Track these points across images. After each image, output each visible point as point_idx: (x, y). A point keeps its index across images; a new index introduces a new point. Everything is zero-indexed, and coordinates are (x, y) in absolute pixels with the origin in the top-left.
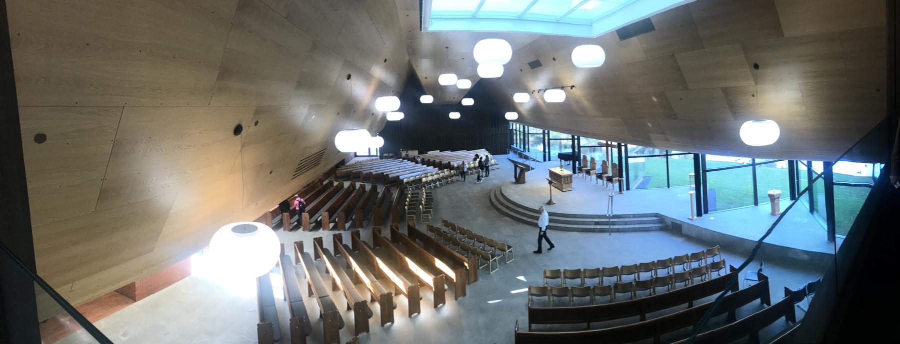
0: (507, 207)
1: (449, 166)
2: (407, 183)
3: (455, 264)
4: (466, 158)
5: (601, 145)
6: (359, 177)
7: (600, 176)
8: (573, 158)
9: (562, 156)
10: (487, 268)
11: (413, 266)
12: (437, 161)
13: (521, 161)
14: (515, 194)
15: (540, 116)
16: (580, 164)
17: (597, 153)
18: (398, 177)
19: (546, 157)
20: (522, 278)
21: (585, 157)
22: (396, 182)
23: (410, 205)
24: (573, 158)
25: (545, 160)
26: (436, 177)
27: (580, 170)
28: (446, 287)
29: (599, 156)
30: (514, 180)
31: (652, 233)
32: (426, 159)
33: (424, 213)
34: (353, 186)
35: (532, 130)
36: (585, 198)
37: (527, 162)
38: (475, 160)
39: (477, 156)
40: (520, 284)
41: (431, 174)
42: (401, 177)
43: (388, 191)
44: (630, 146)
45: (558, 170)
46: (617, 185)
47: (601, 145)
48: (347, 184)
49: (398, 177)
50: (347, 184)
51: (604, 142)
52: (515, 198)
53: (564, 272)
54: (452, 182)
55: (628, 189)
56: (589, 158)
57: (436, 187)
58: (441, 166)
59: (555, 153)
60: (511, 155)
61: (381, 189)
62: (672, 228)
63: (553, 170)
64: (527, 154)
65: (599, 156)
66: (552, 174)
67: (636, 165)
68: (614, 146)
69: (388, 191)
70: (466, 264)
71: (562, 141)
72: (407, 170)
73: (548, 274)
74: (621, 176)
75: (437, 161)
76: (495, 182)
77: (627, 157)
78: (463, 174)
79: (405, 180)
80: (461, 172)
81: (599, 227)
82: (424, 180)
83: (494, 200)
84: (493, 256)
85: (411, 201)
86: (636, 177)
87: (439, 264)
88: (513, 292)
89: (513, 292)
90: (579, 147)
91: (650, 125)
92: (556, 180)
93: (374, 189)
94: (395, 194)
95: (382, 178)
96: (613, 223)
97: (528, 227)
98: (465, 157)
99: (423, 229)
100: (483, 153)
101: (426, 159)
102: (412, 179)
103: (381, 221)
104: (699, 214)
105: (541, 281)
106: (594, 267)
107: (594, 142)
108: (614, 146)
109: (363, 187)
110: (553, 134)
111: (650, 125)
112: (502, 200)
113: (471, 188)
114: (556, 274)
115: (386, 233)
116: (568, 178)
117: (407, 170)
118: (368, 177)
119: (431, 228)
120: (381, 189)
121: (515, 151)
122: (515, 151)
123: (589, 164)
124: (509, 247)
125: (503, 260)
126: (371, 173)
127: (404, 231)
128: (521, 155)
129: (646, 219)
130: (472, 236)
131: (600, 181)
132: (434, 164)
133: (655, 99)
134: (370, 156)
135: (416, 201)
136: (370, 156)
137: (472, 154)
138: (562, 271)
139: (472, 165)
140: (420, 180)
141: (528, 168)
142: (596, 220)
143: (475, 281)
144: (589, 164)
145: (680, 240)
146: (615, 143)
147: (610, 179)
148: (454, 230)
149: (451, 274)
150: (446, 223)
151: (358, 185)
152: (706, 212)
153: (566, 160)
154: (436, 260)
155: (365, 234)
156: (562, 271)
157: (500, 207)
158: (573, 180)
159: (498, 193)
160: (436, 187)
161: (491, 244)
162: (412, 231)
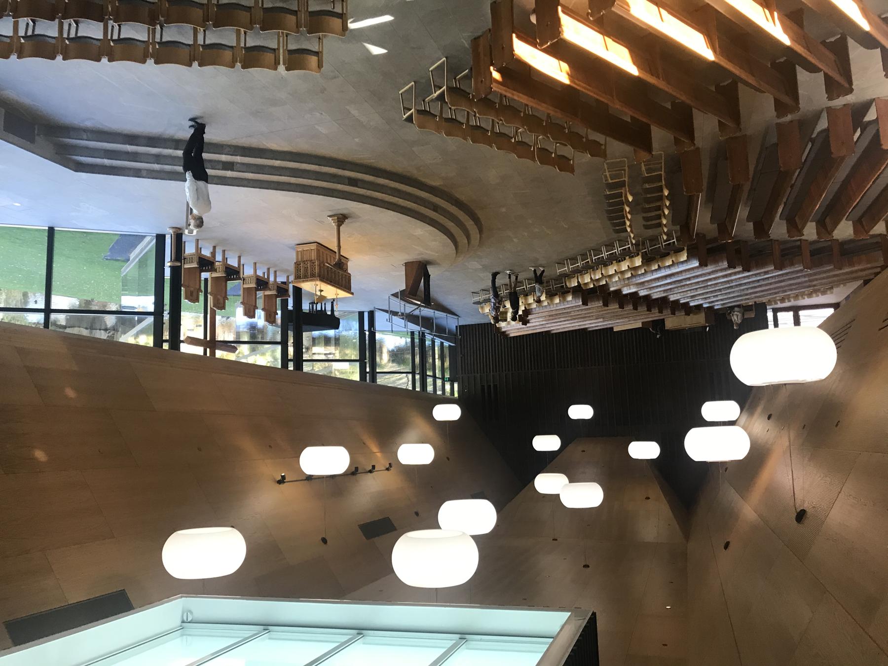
0: (435, 208)
1: (586, 294)
2: (678, 251)
3: (522, 76)
4: (550, 316)
5: (229, 346)
6: (813, 253)
7: (232, 273)
8: (302, 320)
9: (333, 322)
11: (619, 57)
13: (427, 312)
14: (424, 240)
15: (375, 414)
16: (285, 303)
18: (703, 264)
20: (376, 51)
21: (270, 318)
22: (706, 251)
23: (661, 198)
24: (302, 320)
25: (371, 314)
26: (611, 270)
27: (282, 290)
28: (533, 19)
29: (234, 322)
30: (431, 270)
32: (643, 309)
33: (622, 185)
34: (825, 224)
35: (403, 381)
36: (265, 224)
38: (527, 312)
39: (524, 320)
40: (376, 35)
41: (621, 275)
44: (147, 340)
45: (330, 291)
46: (189, 249)
47: (229, 346)
48: (844, 230)
49: (703, 264)
50: (844, 230)
51: (219, 354)
52: (421, 230)
53: (276, 64)
54: (574, 260)
56: (260, 314)
57: (610, 246)
59: (349, 330)
60: (452, 323)
61: (742, 226)
63: (342, 294)
64: (416, 328)
65: (234, 322)
66: (343, 281)
68: (193, 341)
70: (496, 75)
71: (331, 358)
72: (683, 279)
73: (314, 60)
74: (176, 271)
76: (474, 265)
78: (538, 279)
79: (684, 257)
82: (638, 262)
83: (469, 224)
84: (441, 97)
85: (660, 208)
87: (556, 70)
88: (388, 18)
89: (388, 18)
90: (284, 344)
91: (70, 393)
93: (761, 227)
94: (703, 220)
95: (744, 256)
97: (383, 164)
98: (553, 316)
99: (617, 149)
100: (512, 327)
101: (643, 309)
103: (728, 152)
105: (331, 45)
106: (209, 69)
107: (244, 354)
108: (193, 341)
109: (795, 227)
110: (352, 373)
111: (70, 393)
112: (450, 225)
113: (529, 246)
114: (296, 60)
115: (706, 126)
116: (303, 271)
117: (683, 279)
118: (786, 255)
119: (596, 149)
121: (440, 331)
122: (440, 331)
123: (260, 303)
125: (422, 89)
126: (779, 267)
127: (660, 137)
128: (427, 322)
131: (233, 262)
134: (796, 310)
135: (648, 207)
136: (796, 310)
137: (537, 324)
138: (281, 68)
140: (648, 260)
141: (403, 296)
142: (229, 174)
144: (260, 303)
146: (185, 348)
147: (206, 264)
148: (543, 150)
150: (564, 164)
151: (810, 232)
153: (323, 312)
154: (565, 79)
155: (760, 110)
156: (281, 68)
158: (292, 268)
160: (610, 246)
161: (452, 125)
162: (638, 137)
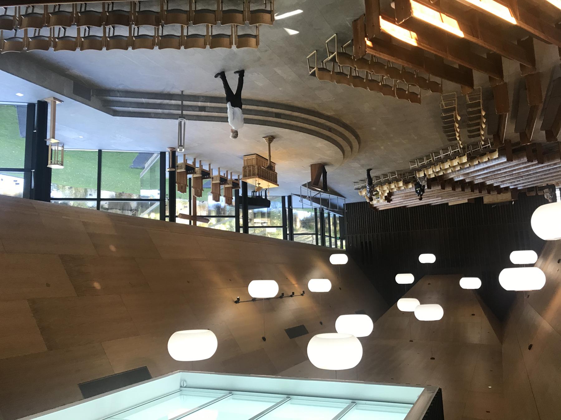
0: (330, 129)
2: (493, 151)
3: (386, 43)
5: (205, 219)
7: (206, 174)
8: (248, 202)
10: (341, 41)
12: (449, 189)
13: (325, 195)
14: (322, 150)
16: (237, 192)
17: (210, 211)
18: (509, 160)
19: (287, 202)
20: (292, 32)
21: (229, 202)
22: (511, 151)
23: (480, 117)
24: (248, 202)
25: (290, 198)
27: (235, 184)
29: (207, 204)
30: (327, 169)
31: (121, 87)
32: (468, 190)
33: (453, 109)
35: (310, 240)
36: (224, 142)
37: (313, 194)
38: (390, 194)
40: (293, 23)
41: (456, 168)
42: (504, 160)
43: (524, 131)
44: (156, 216)
45: (264, 184)
46: (180, 161)
47: (205, 219)
49: (509, 160)
51: (199, 224)
52: (320, 143)
54: (421, 159)
55: (163, 154)
57: (445, 150)
58: (442, 181)
61: (537, 133)
62: (89, 91)
63: (272, 185)
65: (207, 204)
66: (273, 178)
67: (152, 187)
68: (183, 216)
69: (524, 131)
70: (369, 43)
71: (265, 225)
72: (496, 170)
74: (172, 174)
75: (449, 189)
76: (356, 165)
77: (162, 200)
79: (496, 155)
80: (408, 177)
81: (200, 104)
82: (465, 159)
83: (352, 138)
84: (333, 59)
85: (479, 124)
86: (152, 170)
87: (408, 37)
88: (299, 11)
89: (299, 11)
90: (237, 217)
92: (269, 173)
95: (539, 154)
96: (177, 107)
100: (380, 203)
101: (468, 190)
102: (486, 159)
104: (43, 105)
108: (183, 216)
110: (279, 235)
117: (496, 170)
119: (435, 87)
120: (537, 133)
121: (334, 207)
122: (334, 207)
123: (223, 192)
124: (313, 74)
125: (321, 55)
128: (325, 202)
129: (131, 109)
130: (372, 84)
131: (206, 168)
132: (454, 184)
133: (97, 285)
135: (471, 123)
139: (393, 186)
140: (471, 158)
141: (310, 185)
142: (203, 113)
143: (355, 21)
144: (223, 192)
145: (76, 71)
146: (179, 221)
147: (190, 169)
149: (386, 26)
150: (414, 98)
152: (31, 106)
157: (341, 129)
158: (241, 170)
159: (347, 148)
162: (465, 78)
